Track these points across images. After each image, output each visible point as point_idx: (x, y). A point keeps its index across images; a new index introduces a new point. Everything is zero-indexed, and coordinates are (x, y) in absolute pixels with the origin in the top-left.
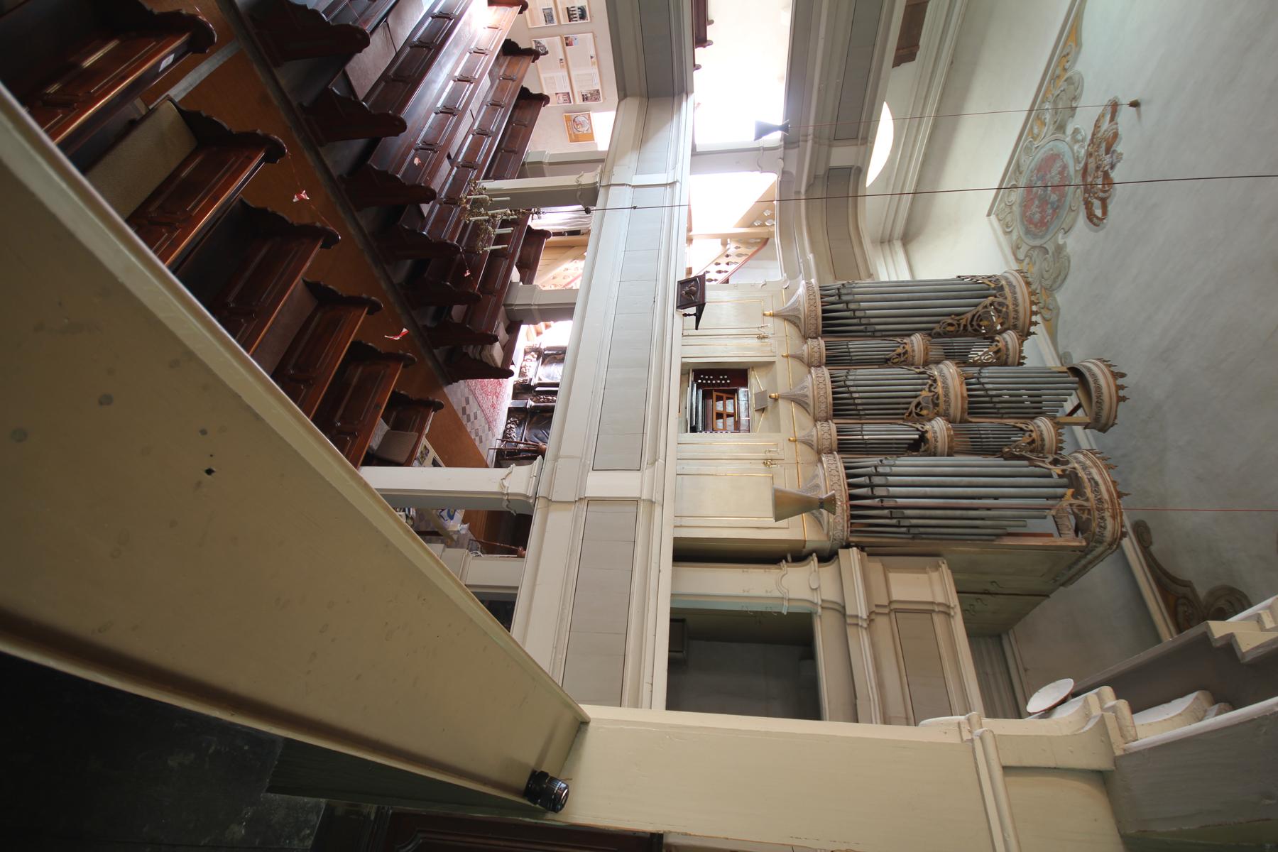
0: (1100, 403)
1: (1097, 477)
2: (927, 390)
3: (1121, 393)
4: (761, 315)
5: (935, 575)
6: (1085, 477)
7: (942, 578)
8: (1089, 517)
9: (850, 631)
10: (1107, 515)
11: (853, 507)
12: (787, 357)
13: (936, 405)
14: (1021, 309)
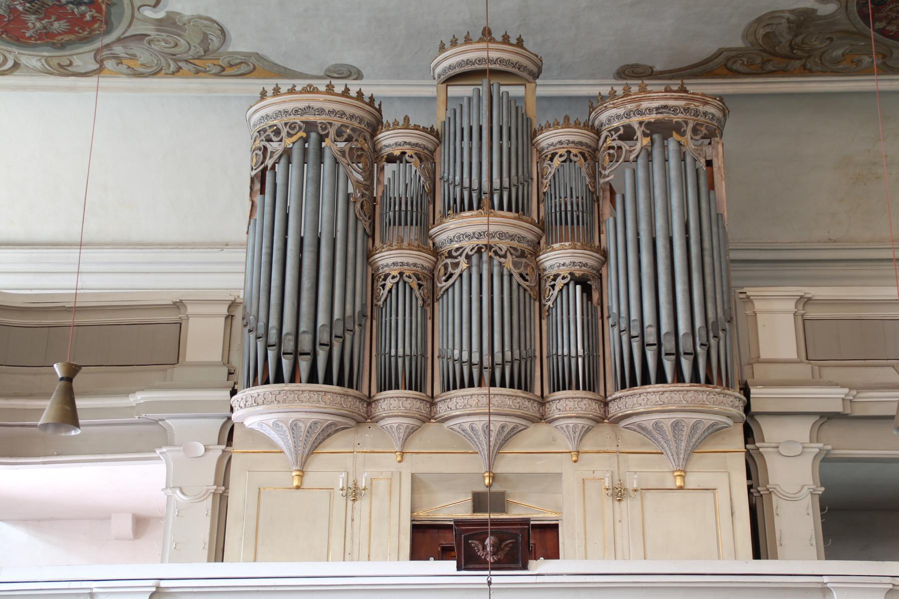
0: (479, 61)
1: (656, 104)
2: (502, 260)
4: (299, 491)
5: (758, 305)
6: (654, 116)
8: (704, 126)
10: (702, 109)
12: (403, 453)
13: (523, 255)
14: (349, 110)
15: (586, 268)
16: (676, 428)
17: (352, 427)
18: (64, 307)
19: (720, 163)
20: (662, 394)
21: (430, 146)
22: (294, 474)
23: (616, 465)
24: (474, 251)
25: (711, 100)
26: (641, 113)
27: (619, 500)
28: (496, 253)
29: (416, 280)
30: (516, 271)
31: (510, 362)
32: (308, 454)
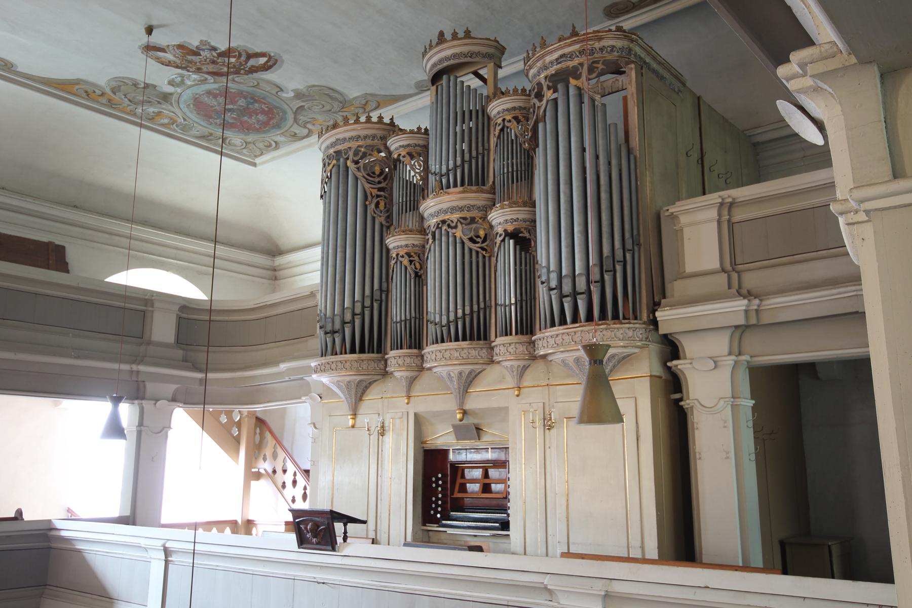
1: (555, 56)
2: (454, 231)
3: (461, 34)
4: (353, 431)
5: (684, 219)
7: (687, 212)
8: (601, 62)
9: (766, 319)
10: (597, 45)
11: (603, 316)
12: (409, 397)
13: (473, 220)
14: (363, 133)
15: (517, 223)
16: (579, 364)
17: (381, 379)
18: (266, 305)
19: (633, 89)
20: (556, 337)
21: (421, 142)
22: (349, 417)
23: (547, 396)
24: (435, 227)
25: (605, 34)
26: (545, 68)
27: (548, 429)
28: (449, 226)
29: (408, 258)
30: (465, 238)
31: (622, 262)
32: (356, 403)
